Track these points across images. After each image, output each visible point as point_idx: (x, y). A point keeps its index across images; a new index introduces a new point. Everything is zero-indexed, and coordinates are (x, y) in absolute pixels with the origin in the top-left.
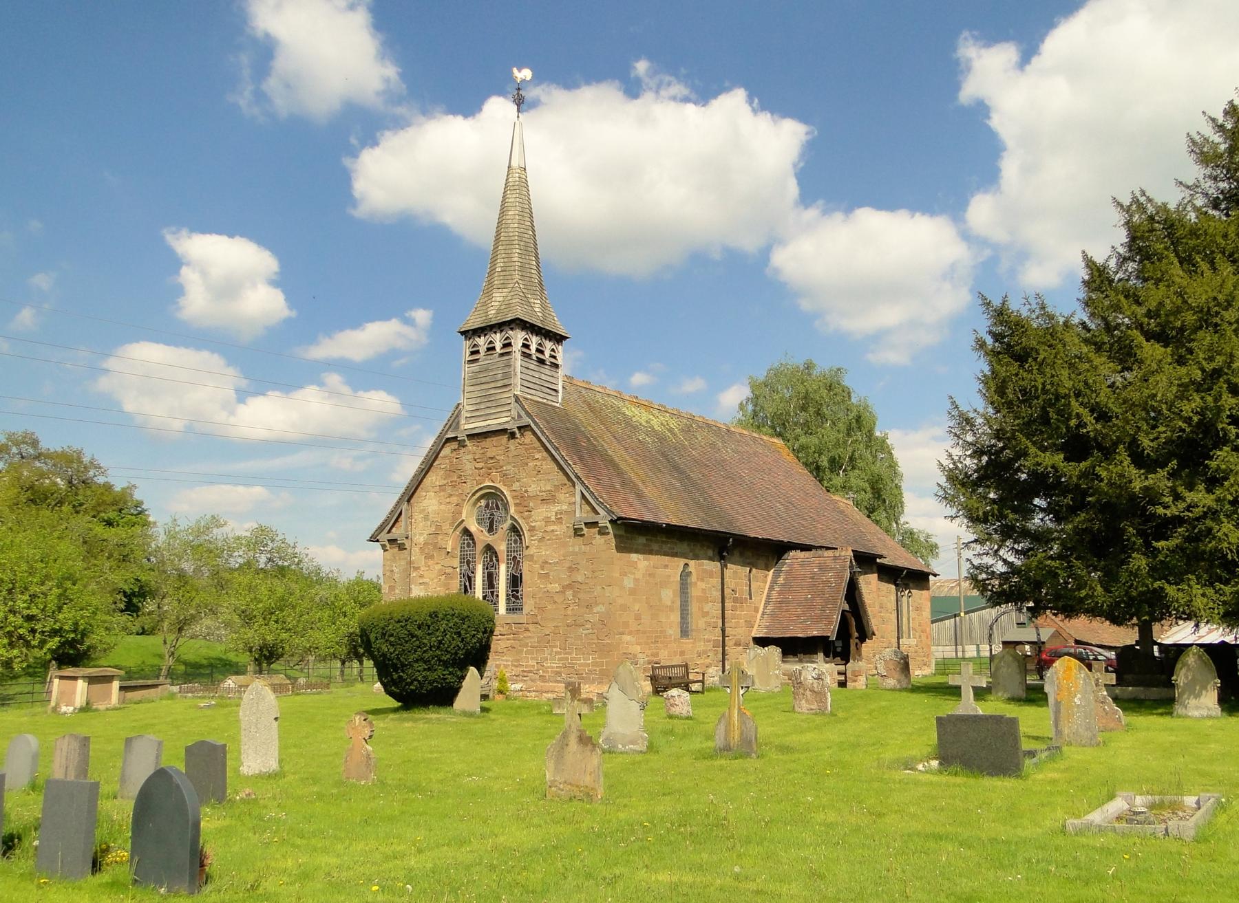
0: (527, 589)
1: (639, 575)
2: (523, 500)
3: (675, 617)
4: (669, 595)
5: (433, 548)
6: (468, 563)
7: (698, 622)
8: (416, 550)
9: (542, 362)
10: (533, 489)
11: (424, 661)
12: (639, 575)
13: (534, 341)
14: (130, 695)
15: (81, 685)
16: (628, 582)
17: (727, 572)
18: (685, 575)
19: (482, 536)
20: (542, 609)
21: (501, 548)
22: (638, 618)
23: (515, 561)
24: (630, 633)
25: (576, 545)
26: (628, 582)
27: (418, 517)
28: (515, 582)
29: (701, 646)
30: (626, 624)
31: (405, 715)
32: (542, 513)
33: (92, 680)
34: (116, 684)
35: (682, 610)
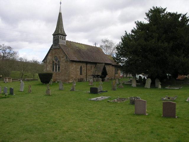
0: (60, 69)
1: (74, 67)
2: (60, 57)
3: (79, 72)
4: (79, 70)
5: (49, 63)
6: (53, 65)
7: (83, 73)
8: (48, 63)
9: (63, 39)
10: (61, 56)
11: (46, 79)
12: (74, 67)
13: (62, 36)
14: (14, 80)
15: (7, 79)
16: (72, 68)
17: (87, 65)
18: (81, 68)
19: (55, 62)
20: (62, 71)
21: (57, 63)
22: (74, 72)
23: (59, 65)
24: (73, 75)
25: (66, 64)
26: (72, 68)
27: (48, 59)
28: (59, 68)
29: (83, 76)
30: (72, 73)
31: (91, 95)
32: (62, 59)
33: (8, 78)
34: (11, 79)
35: (81, 69)
